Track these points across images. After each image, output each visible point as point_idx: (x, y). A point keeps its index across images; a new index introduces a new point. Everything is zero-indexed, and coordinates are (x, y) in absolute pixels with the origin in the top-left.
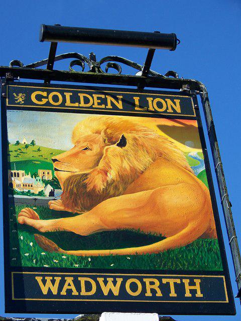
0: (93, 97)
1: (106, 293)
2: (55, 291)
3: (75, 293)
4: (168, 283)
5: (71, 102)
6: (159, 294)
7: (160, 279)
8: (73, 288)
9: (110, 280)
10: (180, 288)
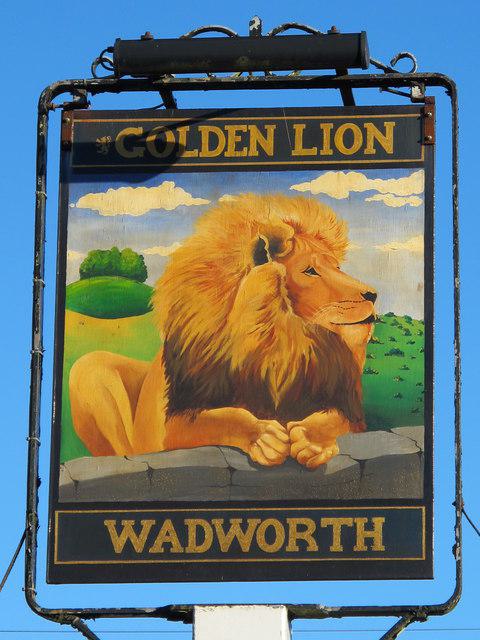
0: (226, 133)
1: (225, 547)
2: (139, 545)
3: (177, 548)
4: (330, 527)
5: (304, 147)
6: (313, 546)
7: (317, 519)
8: (175, 540)
9: (236, 523)
10: (349, 535)
